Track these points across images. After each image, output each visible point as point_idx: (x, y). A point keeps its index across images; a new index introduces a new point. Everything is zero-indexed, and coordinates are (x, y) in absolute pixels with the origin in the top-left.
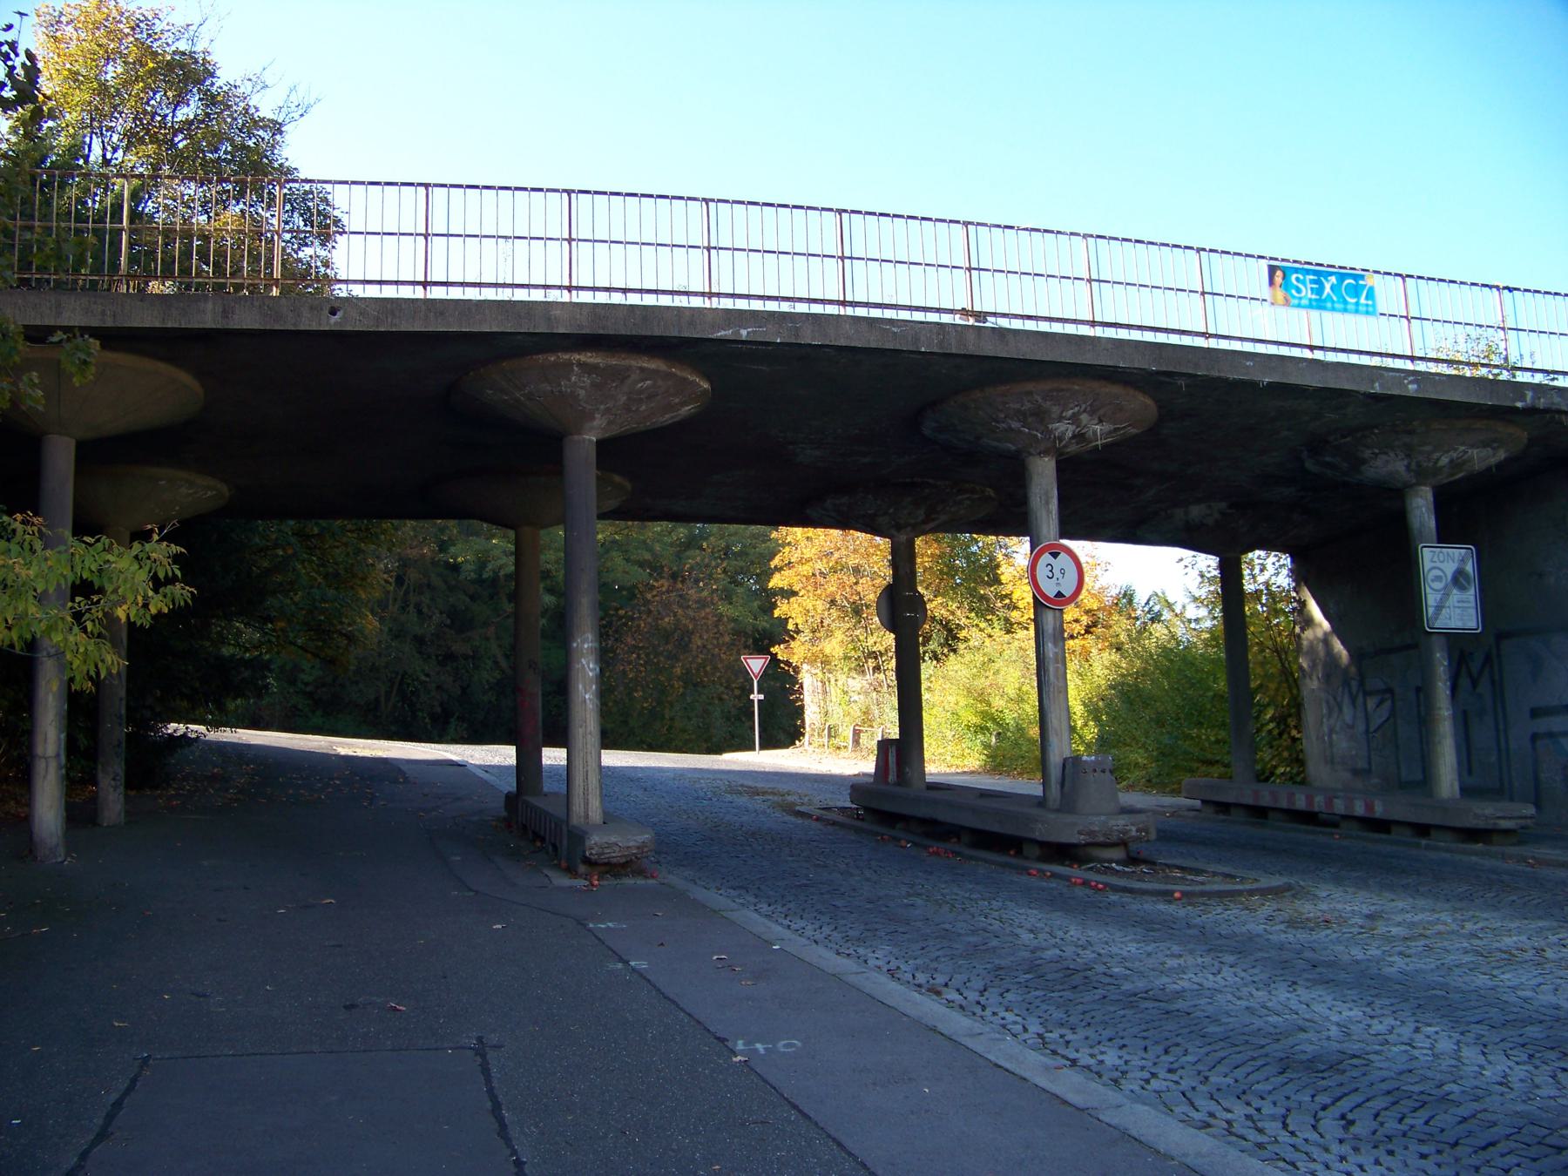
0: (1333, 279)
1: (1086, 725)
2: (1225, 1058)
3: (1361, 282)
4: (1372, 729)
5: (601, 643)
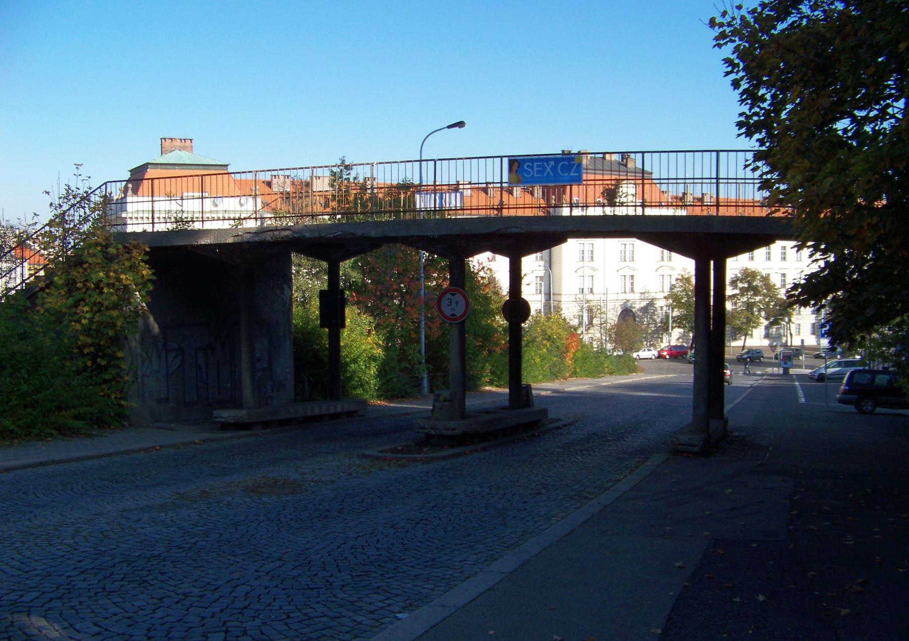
0: (552, 163)
1: (110, 373)
2: (293, 569)
3: (572, 162)
4: (170, 373)
5: (387, 344)
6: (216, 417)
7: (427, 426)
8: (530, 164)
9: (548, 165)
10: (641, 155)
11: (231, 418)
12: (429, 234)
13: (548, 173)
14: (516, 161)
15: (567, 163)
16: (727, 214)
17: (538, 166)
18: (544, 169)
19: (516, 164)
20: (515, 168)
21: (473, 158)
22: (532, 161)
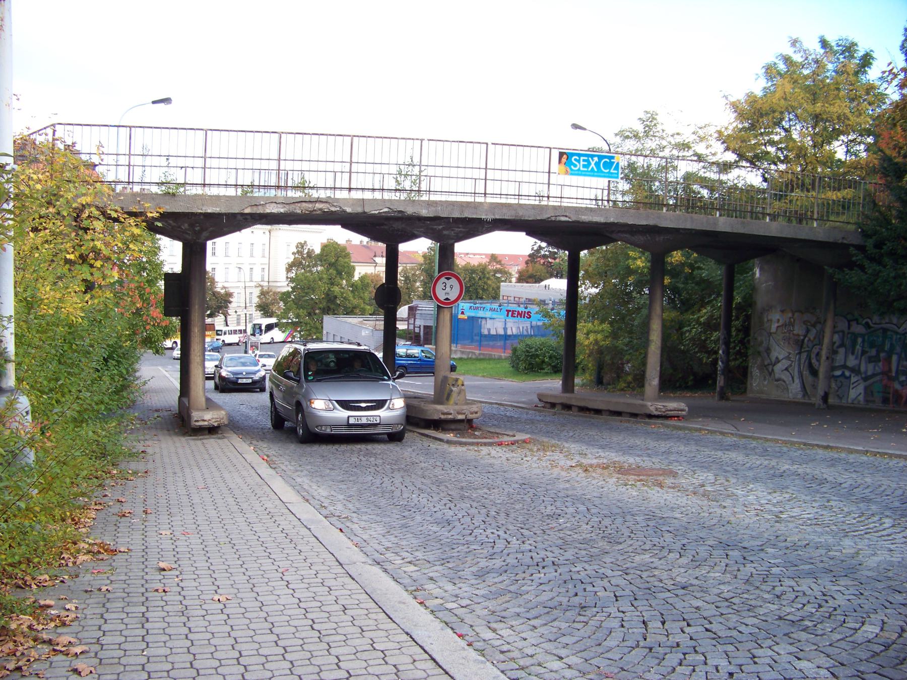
0: (596, 159)
6: (197, 421)
8: (578, 158)
9: (593, 160)
10: (128, 129)
11: (214, 420)
12: (483, 217)
13: (593, 168)
14: (565, 153)
15: (608, 161)
17: (584, 160)
18: (589, 164)
19: (565, 156)
20: (564, 160)
21: (330, 135)
22: (579, 155)
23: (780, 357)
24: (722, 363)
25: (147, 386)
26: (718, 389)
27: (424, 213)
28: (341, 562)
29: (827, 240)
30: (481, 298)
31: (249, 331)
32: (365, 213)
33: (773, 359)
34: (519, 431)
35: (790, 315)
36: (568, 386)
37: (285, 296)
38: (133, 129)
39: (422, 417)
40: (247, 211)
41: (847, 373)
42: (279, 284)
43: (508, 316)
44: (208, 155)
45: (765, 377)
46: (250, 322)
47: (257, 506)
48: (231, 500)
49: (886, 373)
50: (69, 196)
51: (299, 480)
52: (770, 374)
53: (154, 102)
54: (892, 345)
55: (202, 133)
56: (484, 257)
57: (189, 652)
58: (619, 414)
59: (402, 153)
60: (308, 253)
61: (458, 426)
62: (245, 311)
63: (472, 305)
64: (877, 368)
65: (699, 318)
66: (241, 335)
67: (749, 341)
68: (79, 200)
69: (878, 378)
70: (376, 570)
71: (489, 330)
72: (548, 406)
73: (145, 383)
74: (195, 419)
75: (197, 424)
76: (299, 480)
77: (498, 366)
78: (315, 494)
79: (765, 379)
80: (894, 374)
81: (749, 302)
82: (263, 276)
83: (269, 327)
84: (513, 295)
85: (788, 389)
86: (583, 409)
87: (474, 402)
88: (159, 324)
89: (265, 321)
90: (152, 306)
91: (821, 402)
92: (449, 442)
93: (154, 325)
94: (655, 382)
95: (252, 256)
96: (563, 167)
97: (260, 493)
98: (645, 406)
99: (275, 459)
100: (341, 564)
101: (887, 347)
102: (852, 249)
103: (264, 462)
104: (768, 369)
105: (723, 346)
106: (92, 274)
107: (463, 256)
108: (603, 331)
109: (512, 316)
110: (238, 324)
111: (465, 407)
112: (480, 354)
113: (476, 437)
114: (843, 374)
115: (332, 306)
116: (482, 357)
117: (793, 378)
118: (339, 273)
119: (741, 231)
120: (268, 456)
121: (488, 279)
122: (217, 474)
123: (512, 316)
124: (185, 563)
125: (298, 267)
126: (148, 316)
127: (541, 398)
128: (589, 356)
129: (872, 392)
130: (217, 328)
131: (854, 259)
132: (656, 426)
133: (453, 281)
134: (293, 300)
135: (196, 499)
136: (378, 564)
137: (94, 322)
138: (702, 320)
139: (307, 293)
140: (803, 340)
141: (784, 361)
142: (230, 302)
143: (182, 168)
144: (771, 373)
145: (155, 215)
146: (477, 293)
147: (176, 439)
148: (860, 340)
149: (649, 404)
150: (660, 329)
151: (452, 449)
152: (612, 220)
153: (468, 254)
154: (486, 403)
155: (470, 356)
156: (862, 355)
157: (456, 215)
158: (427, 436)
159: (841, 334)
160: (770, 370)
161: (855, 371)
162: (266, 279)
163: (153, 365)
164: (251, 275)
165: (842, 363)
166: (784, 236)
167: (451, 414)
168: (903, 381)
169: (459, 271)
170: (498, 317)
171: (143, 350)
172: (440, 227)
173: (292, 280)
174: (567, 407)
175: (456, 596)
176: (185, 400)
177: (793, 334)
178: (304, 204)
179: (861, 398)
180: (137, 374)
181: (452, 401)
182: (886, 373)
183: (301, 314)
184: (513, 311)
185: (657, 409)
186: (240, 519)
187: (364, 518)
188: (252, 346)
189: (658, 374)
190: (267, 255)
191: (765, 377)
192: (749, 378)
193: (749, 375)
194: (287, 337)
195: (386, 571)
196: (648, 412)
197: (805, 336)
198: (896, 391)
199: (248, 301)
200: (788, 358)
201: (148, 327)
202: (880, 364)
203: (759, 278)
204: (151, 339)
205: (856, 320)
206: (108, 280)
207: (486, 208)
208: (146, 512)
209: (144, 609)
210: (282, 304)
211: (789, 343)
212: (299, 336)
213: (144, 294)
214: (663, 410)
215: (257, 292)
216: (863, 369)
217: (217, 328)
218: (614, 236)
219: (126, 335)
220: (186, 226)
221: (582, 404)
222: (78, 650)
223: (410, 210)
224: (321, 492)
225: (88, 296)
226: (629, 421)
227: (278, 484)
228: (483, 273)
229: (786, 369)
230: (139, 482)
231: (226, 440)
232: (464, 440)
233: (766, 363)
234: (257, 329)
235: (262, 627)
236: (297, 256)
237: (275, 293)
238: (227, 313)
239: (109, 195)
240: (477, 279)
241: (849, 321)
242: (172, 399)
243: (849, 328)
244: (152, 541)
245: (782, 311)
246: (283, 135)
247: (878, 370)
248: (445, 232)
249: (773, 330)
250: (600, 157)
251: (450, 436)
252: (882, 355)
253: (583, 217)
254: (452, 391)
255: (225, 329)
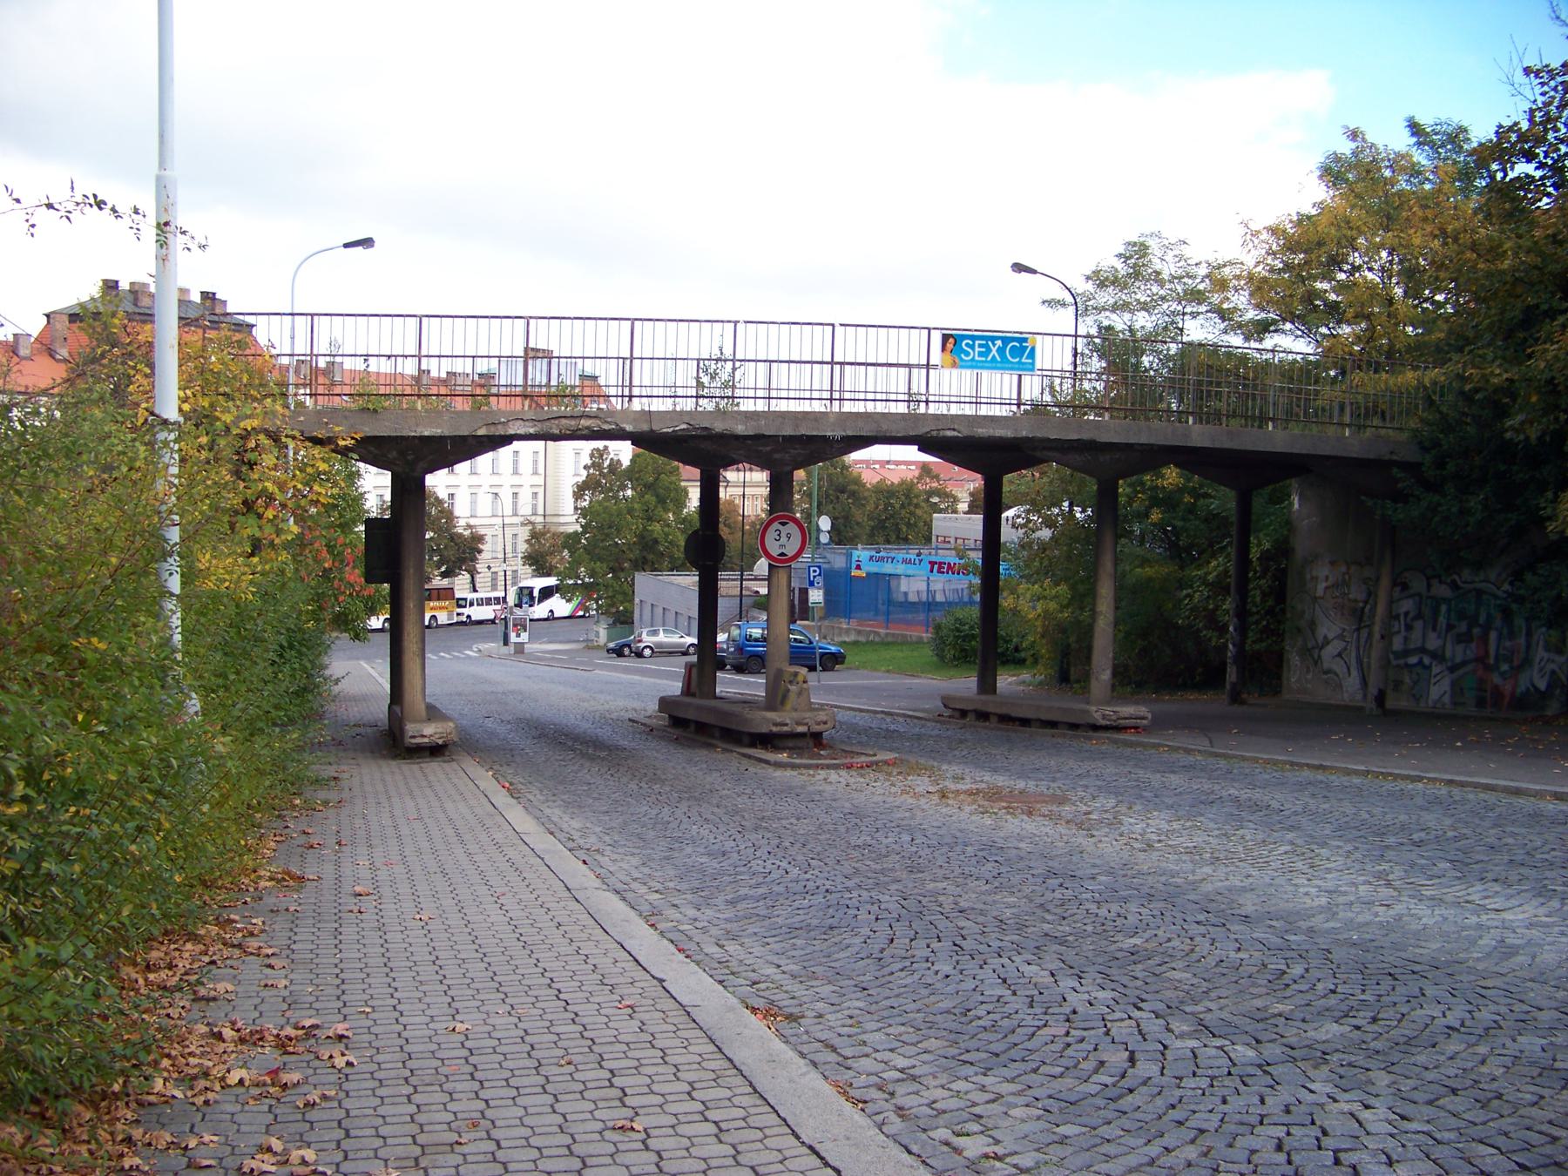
0: (999, 343)
6: (414, 737)
7: (788, 721)
14: (951, 336)
16: (855, 410)
17: (980, 346)
18: (989, 350)
19: (951, 340)
20: (949, 346)
22: (973, 338)
23: (1331, 636)
24: (1234, 645)
25: (336, 689)
26: (1228, 687)
27: (740, 429)
28: (684, 1003)
29: (1365, 456)
30: (906, 540)
31: (511, 600)
32: (652, 431)
33: (1320, 640)
34: (883, 748)
35: (1343, 569)
36: (987, 684)
37: (571, 541)
38: (316, 318)
39: (746, 730)
40: (481, 432)
41: (1426, 661)
42: (562, 520)
43: (932, 571)
44: (424, 352)
45: (1308, 668)
46: (514, 584)
47: (483, 837)
48: (450, 832)
49: (1481, 660)
50: (228, 418)
51: (548, 811)
52: (1316, 663)
53: (346, 246)
54: (1489, 615)
55: (413, 322)
56: (913, 467)
57: (413, 1121)
58: (1053, 724)
59: (706, 343)
60: (610, 465)
61: (800, 743)
62: (504, 567)
63: (874, 553)
64: (1468, 652)
65: (1207, 574)
66: (498, 607)
67: (1283, 611)
68: (242, 425)
69: (1470, 667)
70: (615, 898)
71: (906, 594)
72: (957, 714)
73: (337, 681)
74: (410, 734)
75: (413, 741)
76: (548, 811)
77: (915, 654)
78: (565, 826)
79: (1308, 671)
80: (1492, 661)
81: (1283, 550)
82: (535, 507)
83: (546, 593)
84: (953, 534)
85: (1341, 686)
86: (1005, 719)
87: (822, 707)
88: (358, 593)
89: (539, 583)
90: (347, 565)
91: (1374, 705)
92: (779, 765)
93: (351, 594)
94: (1106, 676)
95: (516, 472)
96: (948, 357)
97: (489, 823)
98: (1087, 712)
99: (520, 786)
100: (569, 890)
101: (1482, 620)
102: (1395, 470)
103: (504, 791)
104: (1311, 654)
105: (1235, 620)
106: (260, 527)
107: (877, 466)
108: (1056, 597)
109: (939, 572)
110: (494, 587)
111: (808, 714)
112: (887, 634)
113: (820, 757)
114: (1420, 662)
115: (650, 557)
116: (890, 639)
117: (1349, 669)
118: (662, 501)
119: (1228, 445)
120: (511, 784)
121: (917, 506)
122: (436, 804)
123: (939, 572)
124: (386, 891)
125: (594, 490)
126: (340, 580)
127: (946, 701)
128: (1043, 636)
129: (1462, 689)
130: (458, 595)
131: (1400, 485)
132: (1100, 743)
133: (792, 528)
134: (585, 547)
135: (405, 831)
136: (618, 892)
137: (265, 595)
138: (1210, 578)
139: (607, 535)
140: (1363, 609)
141: (1335, 642)
142: (480, 551)
143: (389, 357)
144: (1317, 661)
145: (349, 442)
146: (898, 530)
147: (383, 763)
148: (1444, 608)
149: (1094, 708)
150: (1111, 595)
151: (778, 773)
152: (1024, 434)
153: (888, 462)
154: (868, 711)
155: (871, 638)
156: (1447, 631)
157: (788, 431)
158: (749, 757)
159: (1417, 598)
160: (1316, 656)
161: (1437, 656)
162: (541, 511)
163: (350, 658)
164: (515, 504)
165: (1419, 644)
166: (1295, 451)
167: (786, 725)
168: (1505, 672)
169: (866, 494)
170: (917, 572)
171: (334, 634)
172: (768, 448)
173: (584, 513)
174: (983, 716)
175: (695, 920)
176: (397, 709)
177: (1349, 600)
178: (564, 421)
179: (1446, 699)
180: (327, 673)
181: (788, 706)
182: (1481, 660)
183: (598, 570)
184: (941, 563)
185: (1104, 717)
186: (459, 852)
187: (620, 850)
188: (515, 625)
189: (1110, 664)
190: (541, 470)
191: (1308, 668)
192: (1285, 669)
193: (1285, 664)
194: (576, 610)
195: (624, 899)
196: (1091, 721)
197: (1366, 602)
198: (1496, 687)
199: (509, 549)
200: (1341, 637)
201: (341, 598)
202: (1473, 645)
203: (1298, 511)
204: (346, 616)
205: (1439, 576)
206: (283, 537)
207: (832, 420)
208: (339, 843)
209: (337, 925)
210: (566, 553)
211: (1343, 614)
212: (595, 606)
213: (335, 546)
214: (1114, 718)
215: (524, 533)
216: (1448, 654)
217: (458, 595)
218: (1038, 454)
219: (307, 612)
220: (394, 453)
221: (1004, 711)
222: (270, 951)
223: (719, 426)
224: (574, 824)
225: (255, 560)
226: (1064, 736)
227: (517, 816)
228: (907, 496)
229: (1339, 655)
230: (331, 813)
231: (454, 765)
232: (798, 761)
233: (1310, 646)
234: (526, 596)
235: (538, 1103)
236: (591, 471)
237: (556, 535)
238: (475, 569)
239: (284, 416)
240: (897, 506)
241: (1428, 579)
242: (380, 710)
243: (1429, 590)
244: (347, 870)
245: (1332, 563)
246: (532, 321)
247: (1470, 654)
248: (777, 456)
249: (1320, 592)
250: (1006, 340)
251: (783, 757)
252: (1476, 631)
253: (980, 430)
254: (788, 690)
255: (471, 596)
